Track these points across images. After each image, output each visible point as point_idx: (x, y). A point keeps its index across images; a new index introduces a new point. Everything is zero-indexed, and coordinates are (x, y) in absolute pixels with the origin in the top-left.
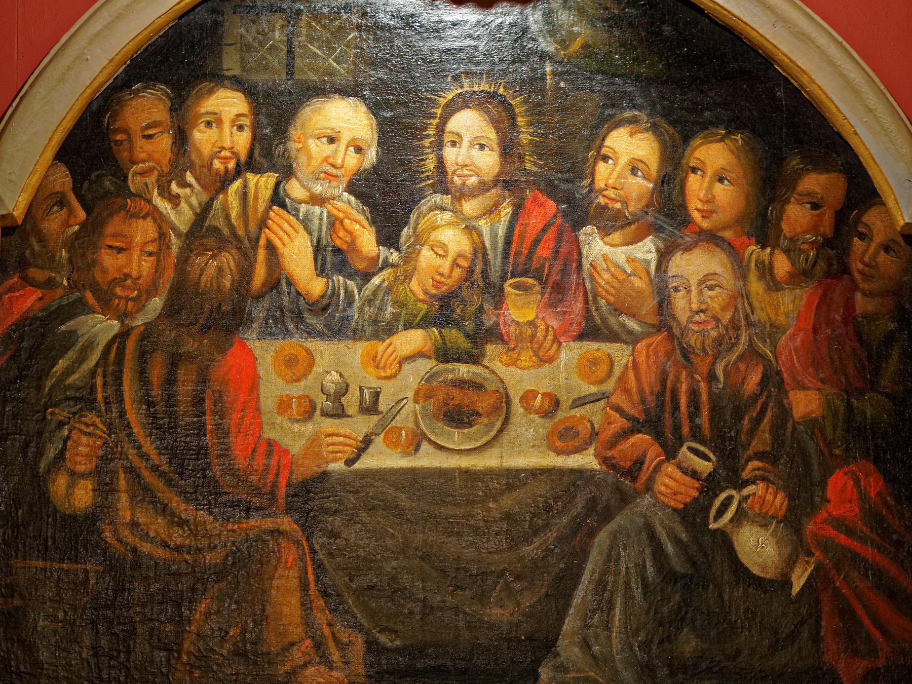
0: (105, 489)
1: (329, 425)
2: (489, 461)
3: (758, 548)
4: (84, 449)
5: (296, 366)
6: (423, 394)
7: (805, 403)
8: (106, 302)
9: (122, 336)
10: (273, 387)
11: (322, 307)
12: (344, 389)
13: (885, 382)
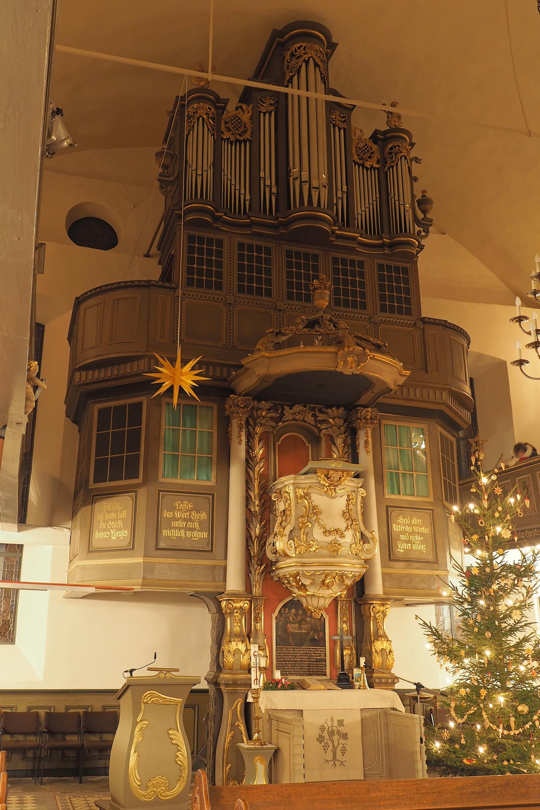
3: (316, 637)
10: (290, 627)
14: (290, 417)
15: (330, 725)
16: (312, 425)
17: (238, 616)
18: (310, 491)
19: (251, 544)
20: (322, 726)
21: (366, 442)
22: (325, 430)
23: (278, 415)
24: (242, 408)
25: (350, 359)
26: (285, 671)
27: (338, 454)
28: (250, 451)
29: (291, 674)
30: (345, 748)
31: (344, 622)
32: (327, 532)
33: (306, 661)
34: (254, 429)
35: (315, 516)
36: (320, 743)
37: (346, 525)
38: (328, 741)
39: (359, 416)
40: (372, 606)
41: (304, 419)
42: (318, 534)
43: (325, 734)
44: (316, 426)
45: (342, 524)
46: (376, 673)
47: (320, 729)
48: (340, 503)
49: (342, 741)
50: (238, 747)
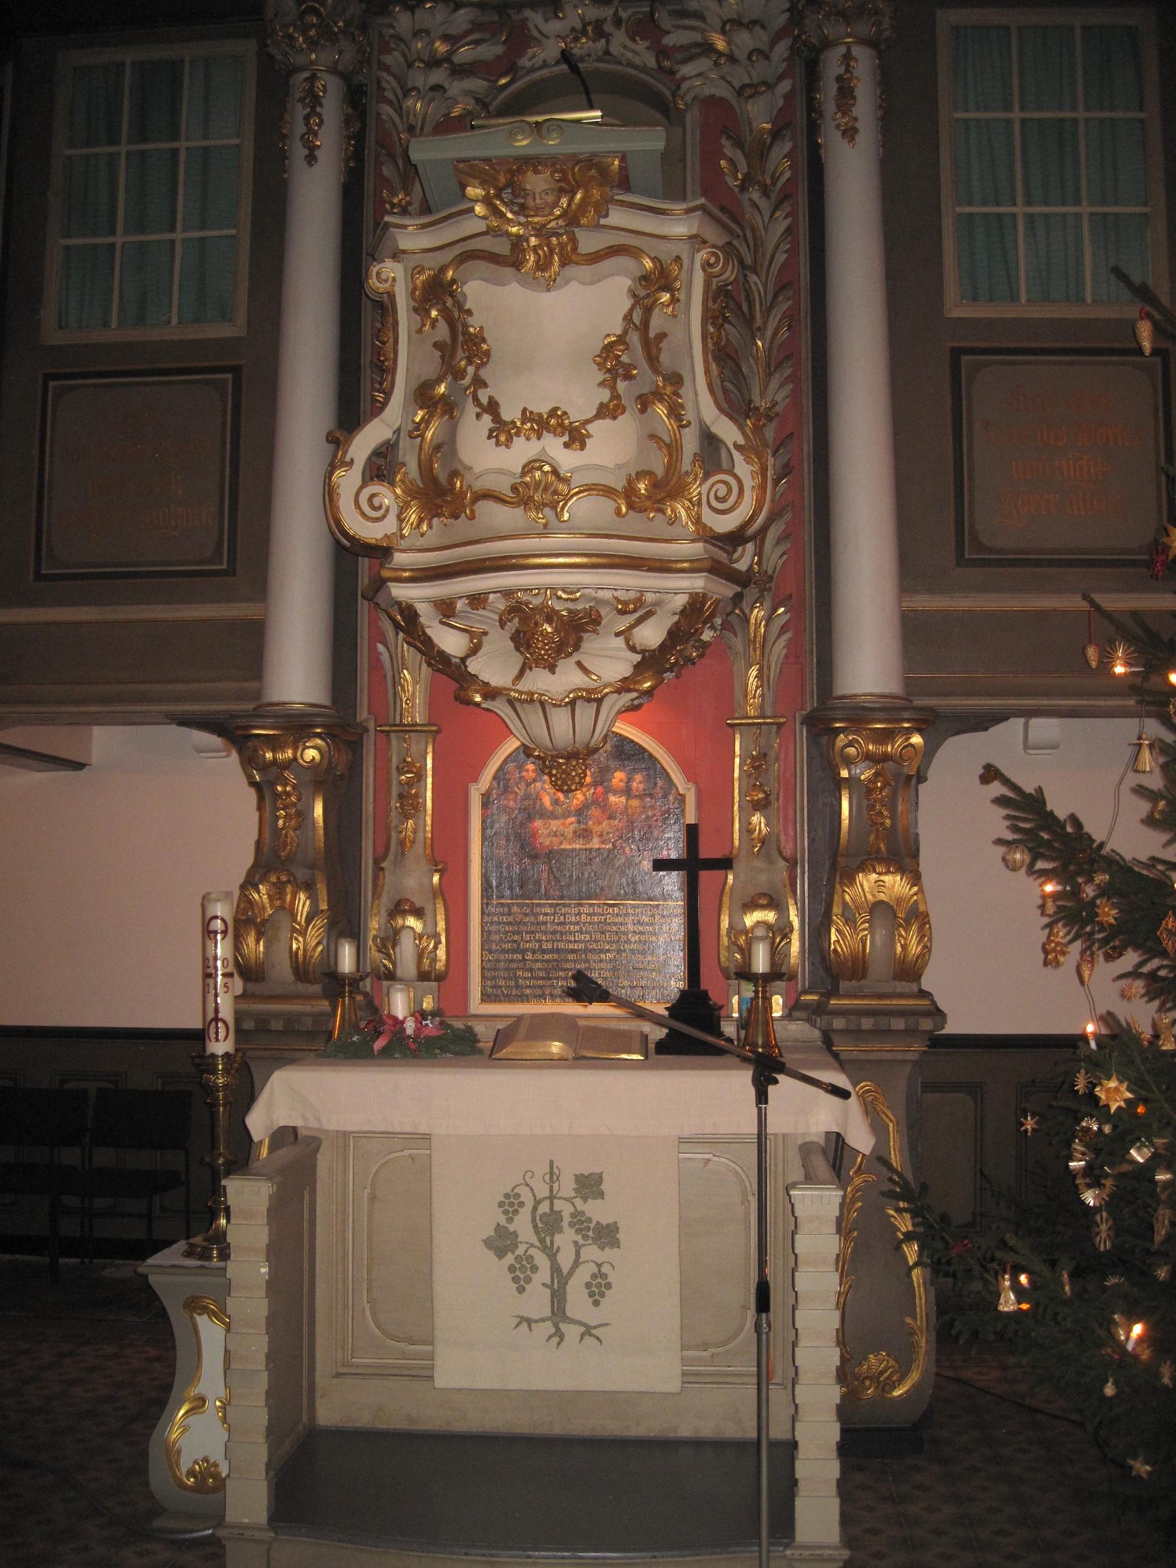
6: (575, 832)
11: (552, 813)
15: (542, 1191)
20: (507, 1196)
30: (604, 1276)
36: (501, 1253)
38: (532, 1251)
41: (607, 52)
43: (523, 1226)
47: (501, 1204)
49: (591, 1252)
50: (1171, 1172)
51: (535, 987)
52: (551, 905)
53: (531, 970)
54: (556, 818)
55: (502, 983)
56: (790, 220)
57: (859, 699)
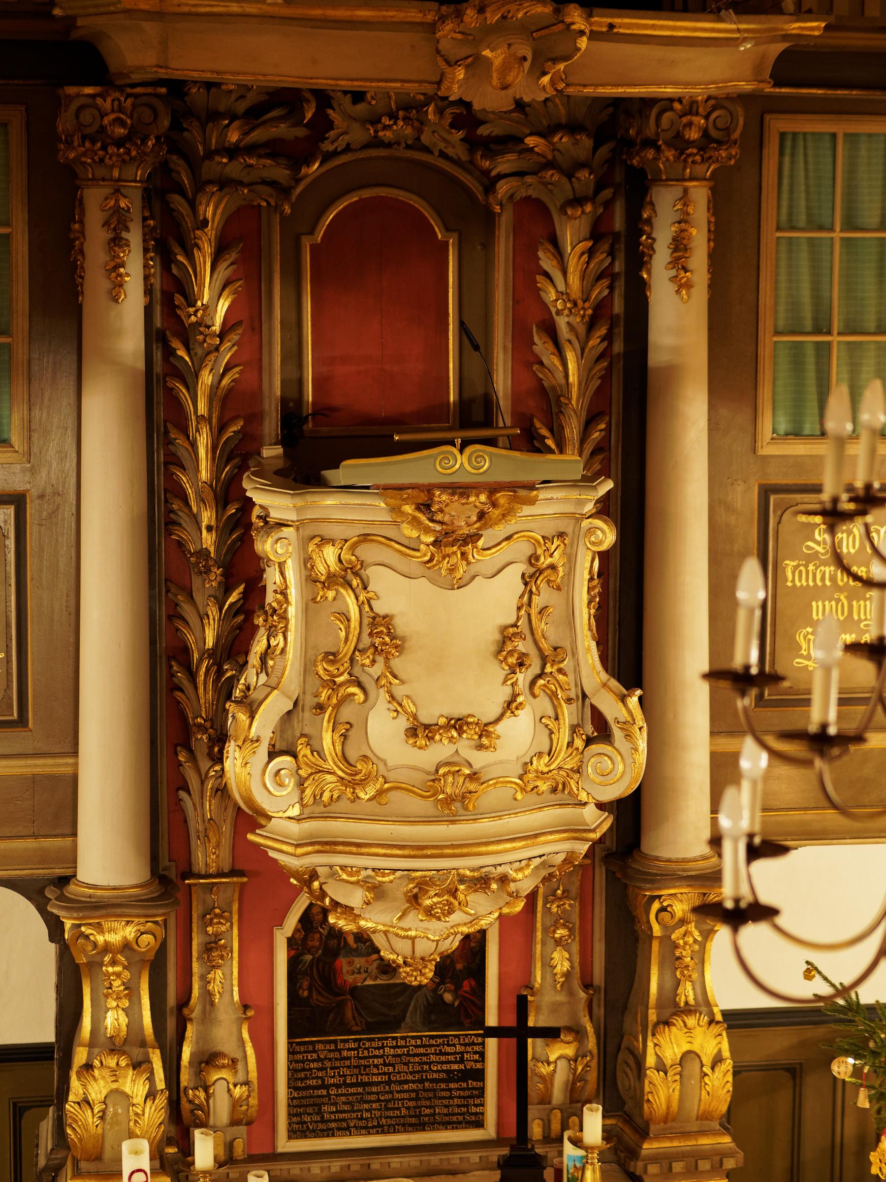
0: (310, 992)
1: (357, 976)
2: (391, 982)
3: (448, 997)
4: (306, 984)
5: (350, 963)
6: (377, 968)
7: (459, 966)
8: (309, 952)
9: (313, 960)
10: (345, 968)
11: (356, 950)
12: (360, 968)
13: (477, 961)
14: (358, 135)
16: (457, 162)
17: (118, 975)
18: (367, 552)
19: (186, 684)
21: (680, 245)
22: (513, 182)
23: (301, 132)
24: (120, 142)
25: (494, 55)
26: (323, 1121)
27: (561, 287)
28: (179, 299)
29: (348, 1128)
31: (558, 942)
32: (420, 731)
33: (406, 1082)
34: (193, 206)
35: (380, 659)
37: (506, 692)
39: (651, 129)
40: (656, 906)
42: (383, 731)
44: (469, 166)
45: (481, 691)
46: (657, 1138)
48: (493, 596)
51: (339, 1120)
52: (355, 1040)
53: (335, 1104)
54: (360, 955)
55: (307, 1118)
56: (605, 344)
57: (673, 866)
